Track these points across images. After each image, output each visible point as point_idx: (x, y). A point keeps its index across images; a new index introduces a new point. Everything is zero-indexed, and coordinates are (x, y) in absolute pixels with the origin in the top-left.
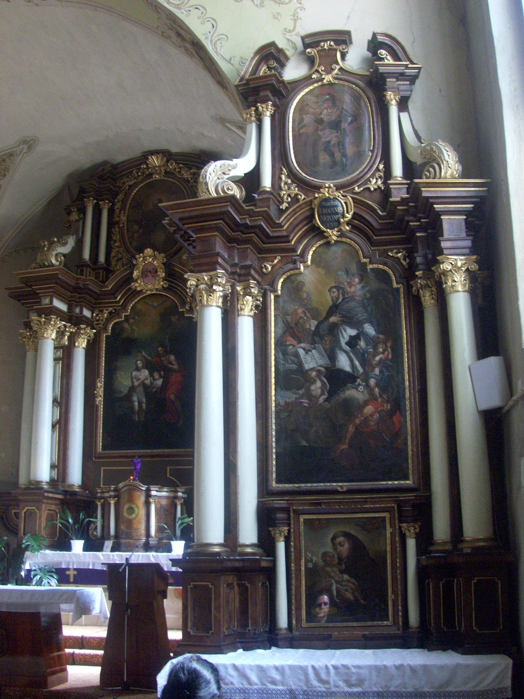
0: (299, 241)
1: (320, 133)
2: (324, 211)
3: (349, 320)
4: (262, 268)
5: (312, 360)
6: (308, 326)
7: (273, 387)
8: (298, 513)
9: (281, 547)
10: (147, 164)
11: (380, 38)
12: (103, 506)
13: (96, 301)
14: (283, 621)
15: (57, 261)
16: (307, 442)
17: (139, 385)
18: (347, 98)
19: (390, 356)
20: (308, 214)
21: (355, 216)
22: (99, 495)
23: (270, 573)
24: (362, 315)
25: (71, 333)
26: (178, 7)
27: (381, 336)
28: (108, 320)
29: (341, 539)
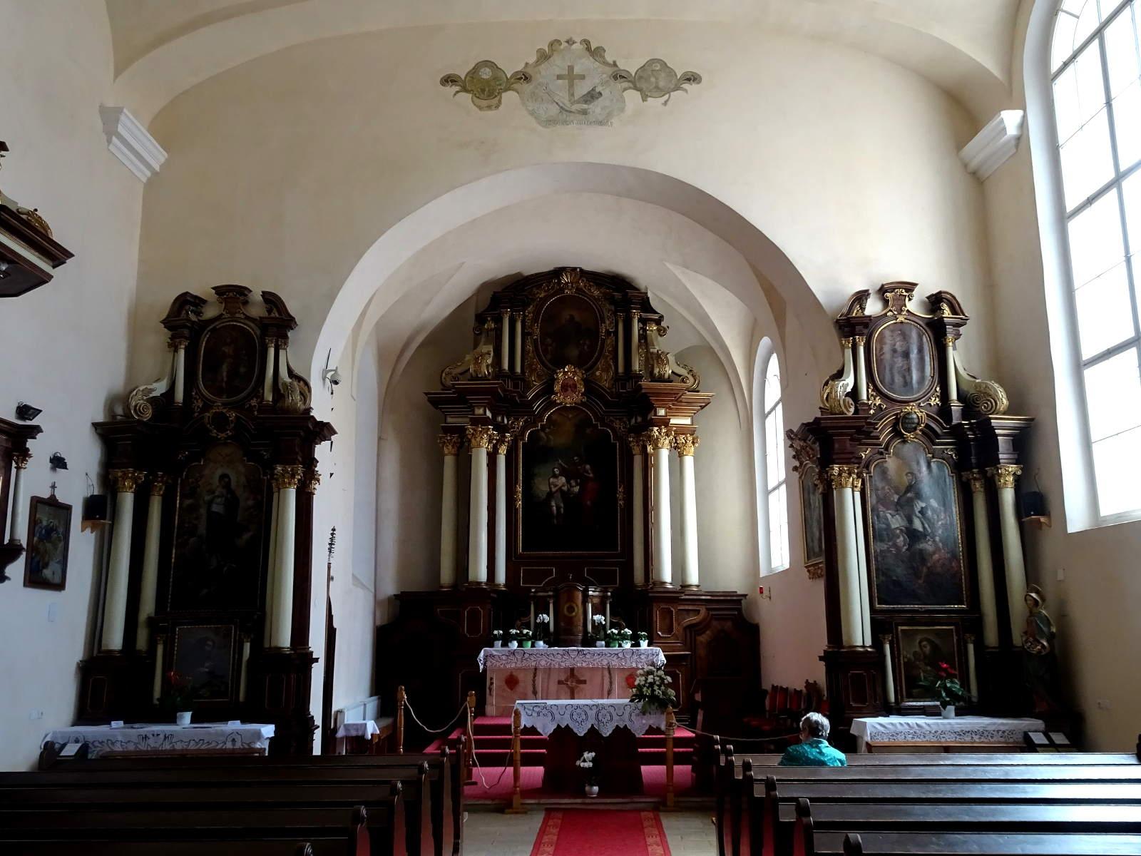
2: (907, 421)
5: (896, 522)
9: (887, 647)
17: (557, 491)
21: (927, 426)
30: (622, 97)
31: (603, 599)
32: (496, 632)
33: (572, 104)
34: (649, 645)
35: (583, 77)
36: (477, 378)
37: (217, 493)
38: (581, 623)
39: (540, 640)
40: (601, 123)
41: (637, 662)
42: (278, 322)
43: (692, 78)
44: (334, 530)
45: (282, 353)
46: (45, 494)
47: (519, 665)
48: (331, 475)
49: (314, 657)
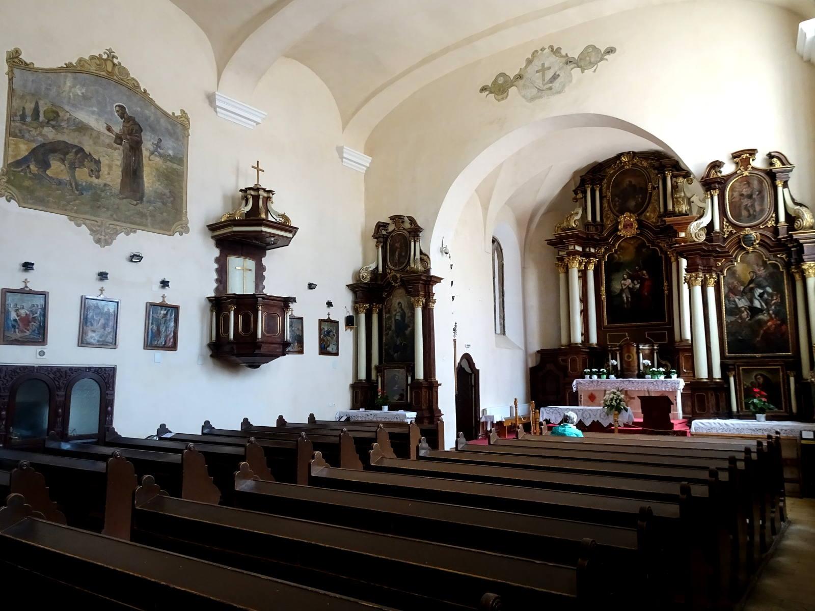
0: (734, 252)
1: (742, 201)
2: (746, 240)
4: (716, 264)
5: (742, 303)
6: (739, 289)
7: (725, 315)
8: (739, 366)
9: (732, 379)
10: (621, 161)
11: (773, 154)
14: (734, 408)
15: (575, 224)
16: (741, 337)
17: (626, 288)
19: (779, 301)
20: (738, 241)
21: (761, 240)
22: (609, 349)
24: (765, 283)
25: (585, 262)
27: (775, 293)
28: (605, 253)
29: (759, 377)
30: (570, 74)
32: (585, 370)
33: (544, 85)
34: (677, 377)
35: (549, 68)
36: (569, 229)
37: (397, 311)
38: (636, 364)
39: (612, 374)
40: (559, 92)
41: (665, 388)
42: (416, 231)
43: (610, 51)
44: (456, 323)
45: (417, 244)
46: (326, 318)
47: (595, 388)
48: (453, 297)
49: (439, 383)
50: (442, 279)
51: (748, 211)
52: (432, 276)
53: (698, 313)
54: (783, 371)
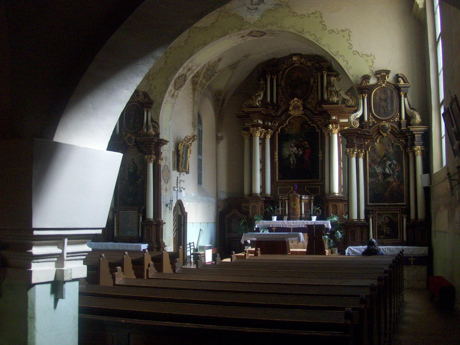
0: (375, 136)
3: (389, 159)
5: (379, 170)
8: (375, 211)
9: (371, 220)
12: (282, 203)
13: (273, 119)
18: (389, 92)
23: (369, 226)
26: (335, 55)
28: (278, 127)
31: (310, 201)
45: (149, 114)
50: (168, 142)
51: (384, 110)
52: (162, 139)
53: (344, 172)
54: (400, 215)
